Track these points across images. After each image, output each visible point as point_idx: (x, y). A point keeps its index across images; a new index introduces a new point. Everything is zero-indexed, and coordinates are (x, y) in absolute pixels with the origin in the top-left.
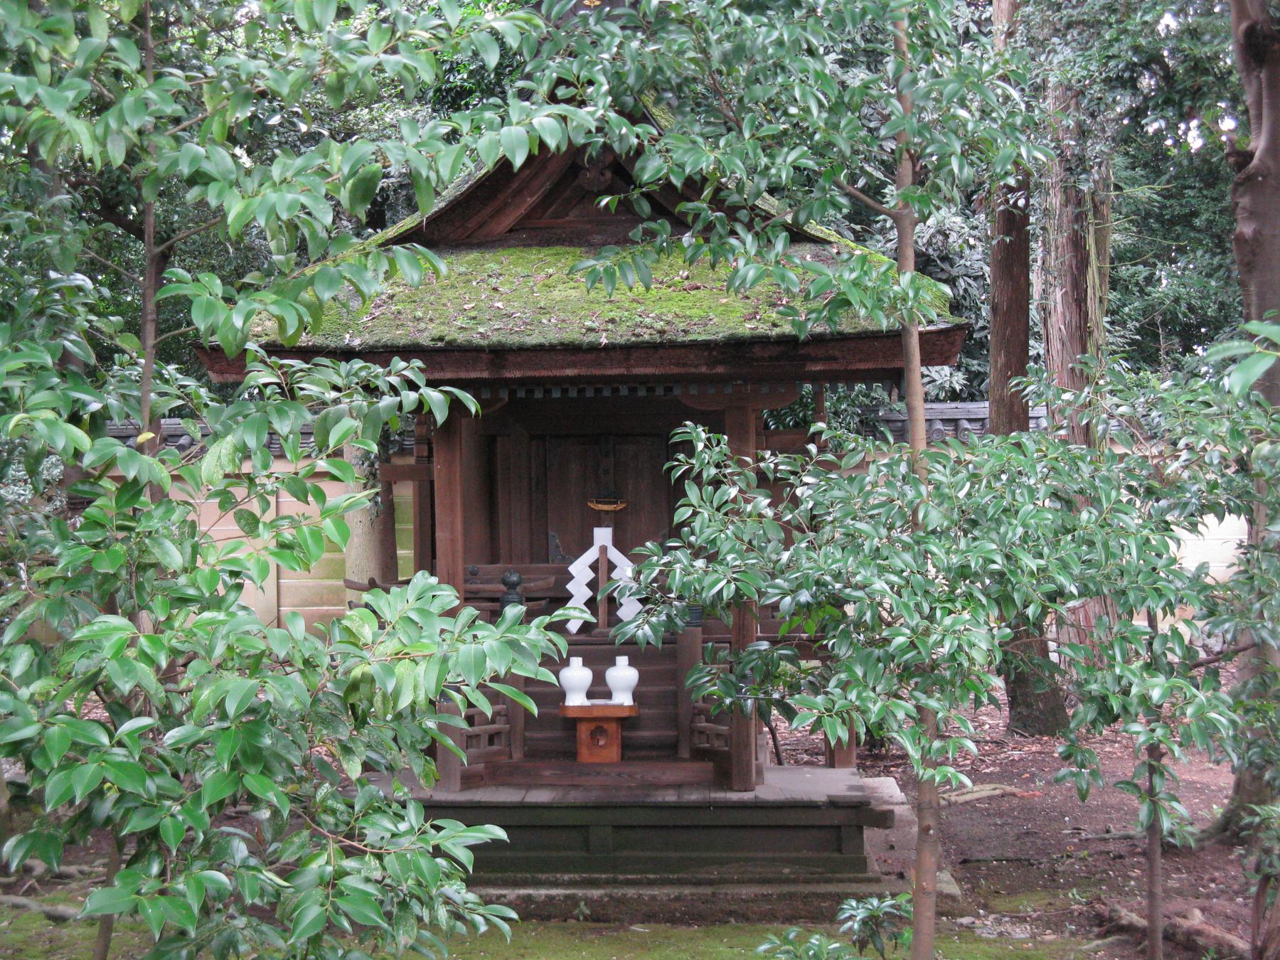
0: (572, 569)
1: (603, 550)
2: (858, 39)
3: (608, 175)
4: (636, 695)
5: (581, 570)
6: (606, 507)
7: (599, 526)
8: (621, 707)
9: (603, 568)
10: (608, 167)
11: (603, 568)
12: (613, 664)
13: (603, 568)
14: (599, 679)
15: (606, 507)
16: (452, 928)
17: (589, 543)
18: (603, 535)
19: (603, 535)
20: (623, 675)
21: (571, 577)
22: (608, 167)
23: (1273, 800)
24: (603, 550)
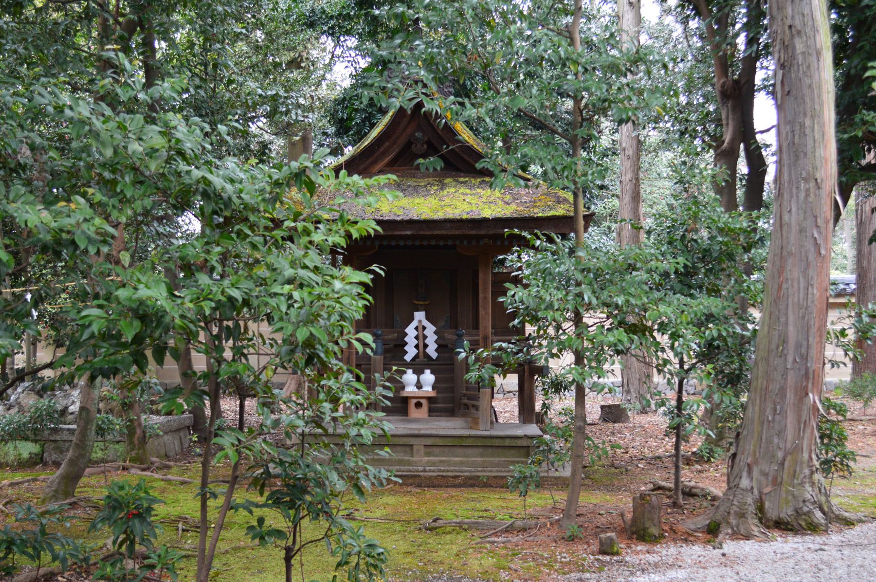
0: (406, 331)
1: (420, 321)
2: (468, 105)
3: (425, 146)
4: (434, 388)
5: (411, 331)
6: (421, 303)
7: (418, 311)
8: (427, 391)
9: (420, 328)
10: (426, 143)
11: (420, 328)
12: (423, 373)
13: (420, 328)
14: (351, 48)
15: (421, 303)
16: (364, 352)
17: (412, 319)
18: (420, 316)
19: (420, 316)
20: (428, 377)
21: (406, 334)
22: (426, 143)
23: (109, 3)
24: (420, 321)
